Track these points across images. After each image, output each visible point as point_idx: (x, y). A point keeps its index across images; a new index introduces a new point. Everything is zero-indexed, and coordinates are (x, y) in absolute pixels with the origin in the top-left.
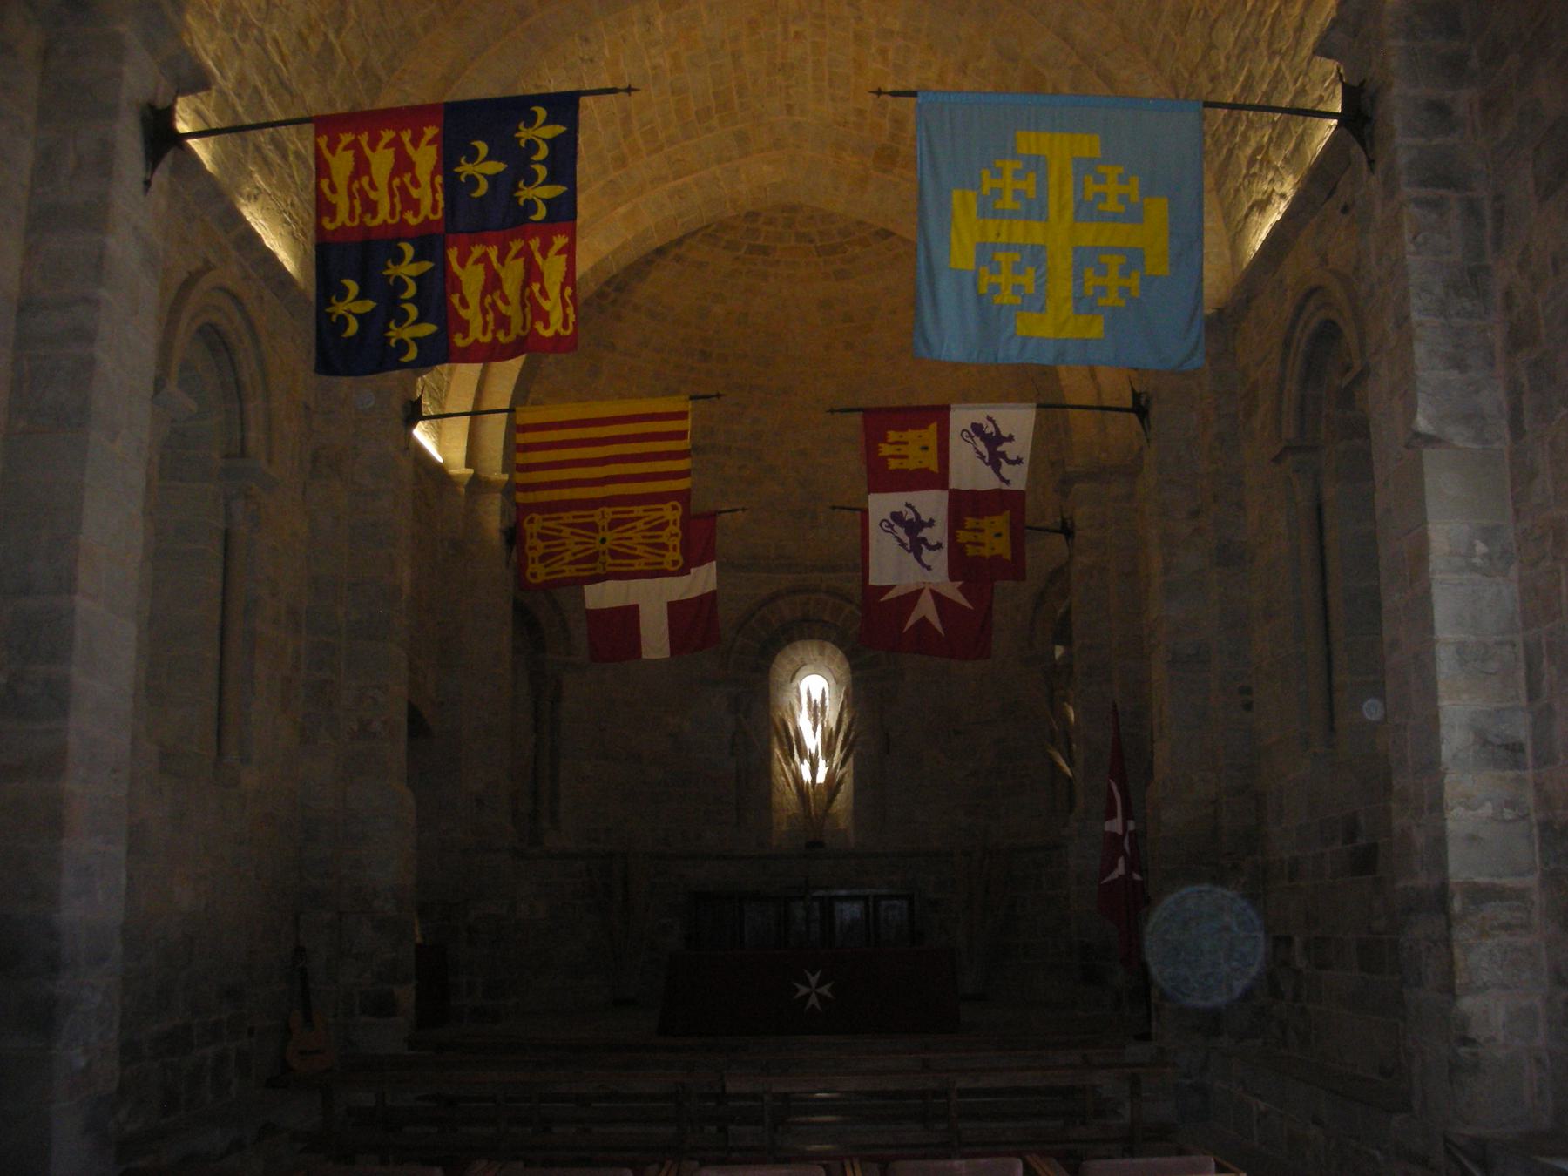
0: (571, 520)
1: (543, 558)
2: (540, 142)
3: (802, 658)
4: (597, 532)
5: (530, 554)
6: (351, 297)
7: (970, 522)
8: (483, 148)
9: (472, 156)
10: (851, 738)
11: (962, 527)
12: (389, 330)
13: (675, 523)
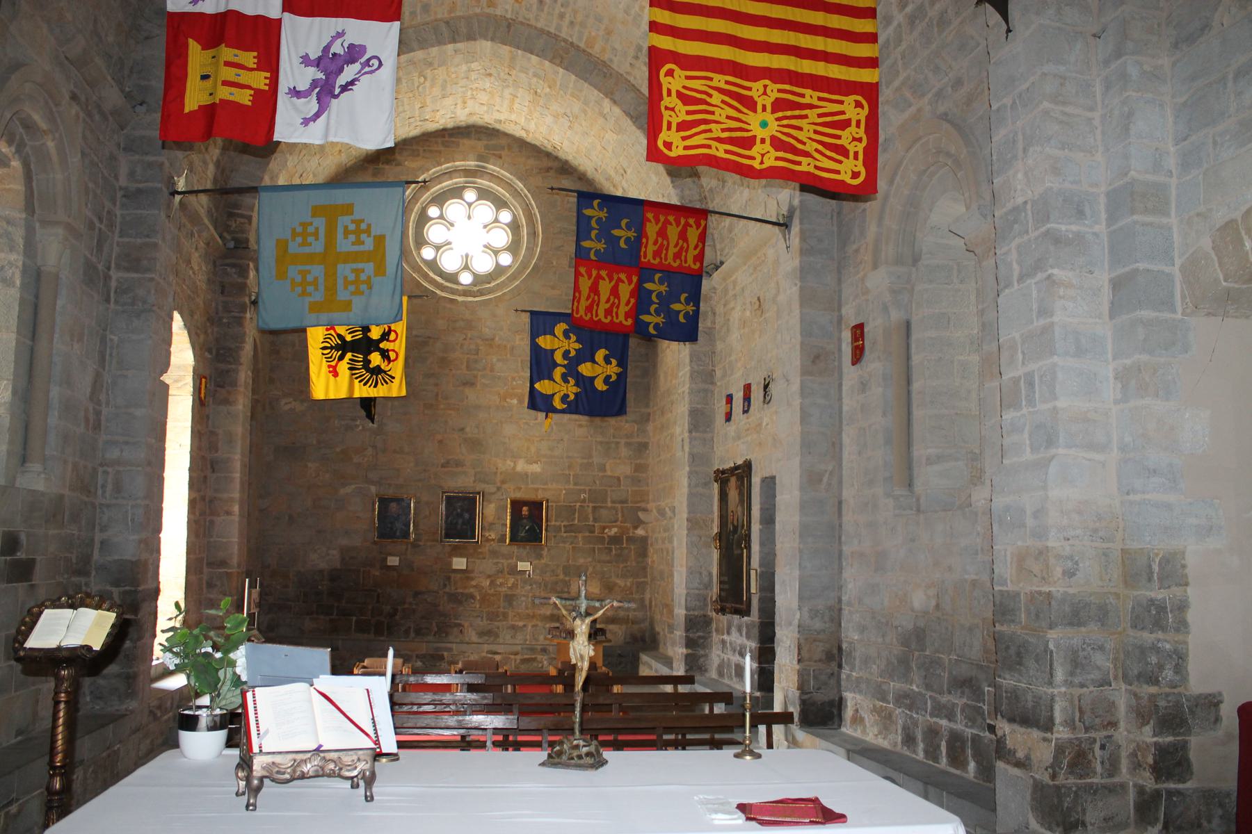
0: (804, 160)
1: (845, 124)
2: (624, 227)
3: (1048, 726)
4: (773, 138)
5: (861, 133)
6: (652, 325)
7: (245, 98)
8: (622, 245)
9: (628, 240)
10: (672, 737)
11: (258, 93)
12: (576, 394)
13: (858, 122)
